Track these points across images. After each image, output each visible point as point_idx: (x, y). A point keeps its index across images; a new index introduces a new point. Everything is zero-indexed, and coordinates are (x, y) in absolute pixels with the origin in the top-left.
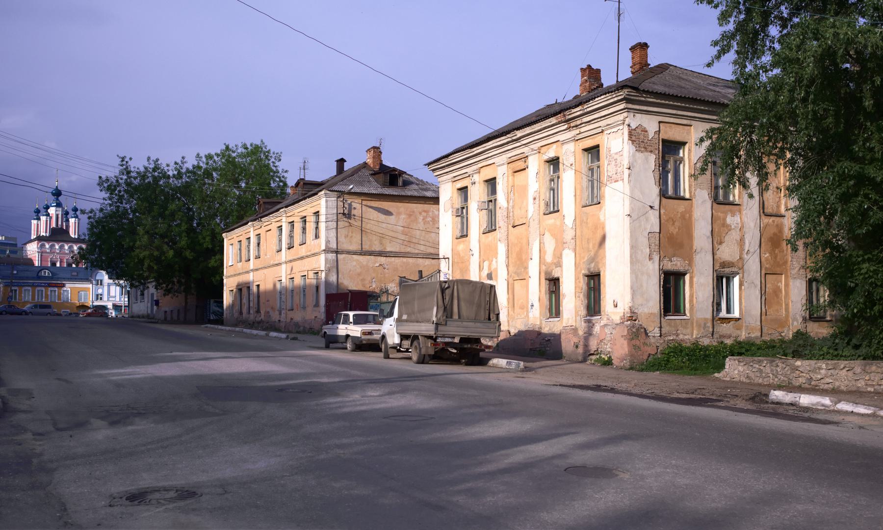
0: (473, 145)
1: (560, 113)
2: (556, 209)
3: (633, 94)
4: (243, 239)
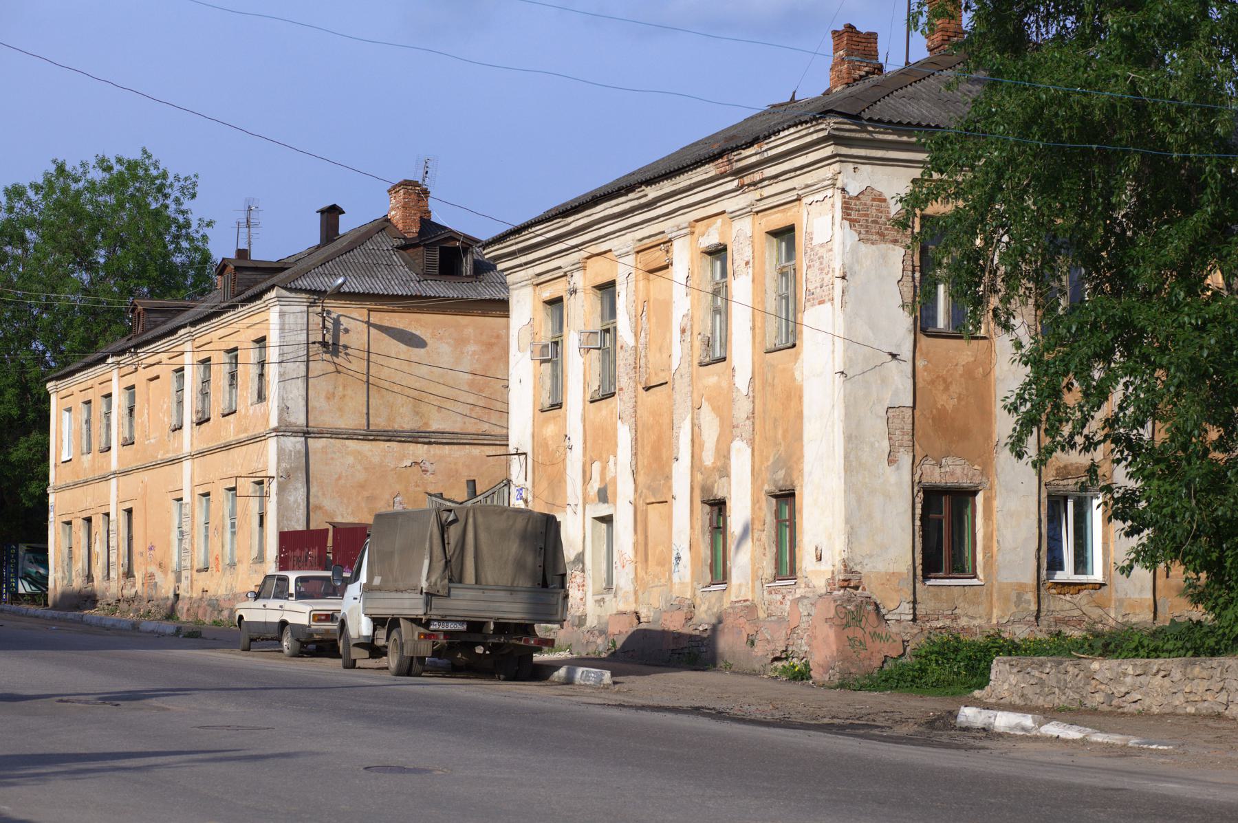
0: (567, 210)
1: (720, 155)
4: (95, 395)
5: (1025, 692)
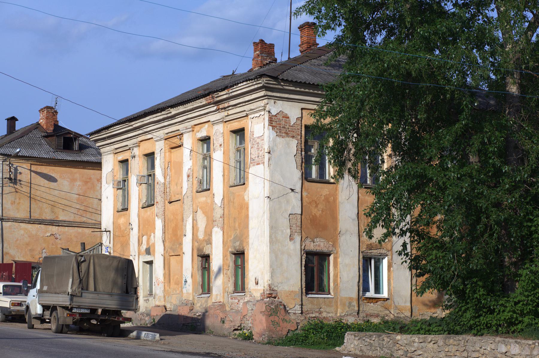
0: (131, 119)
1: (208, 94)
2: (208, 188)
3: (272, 82)
5: (362, 349)
